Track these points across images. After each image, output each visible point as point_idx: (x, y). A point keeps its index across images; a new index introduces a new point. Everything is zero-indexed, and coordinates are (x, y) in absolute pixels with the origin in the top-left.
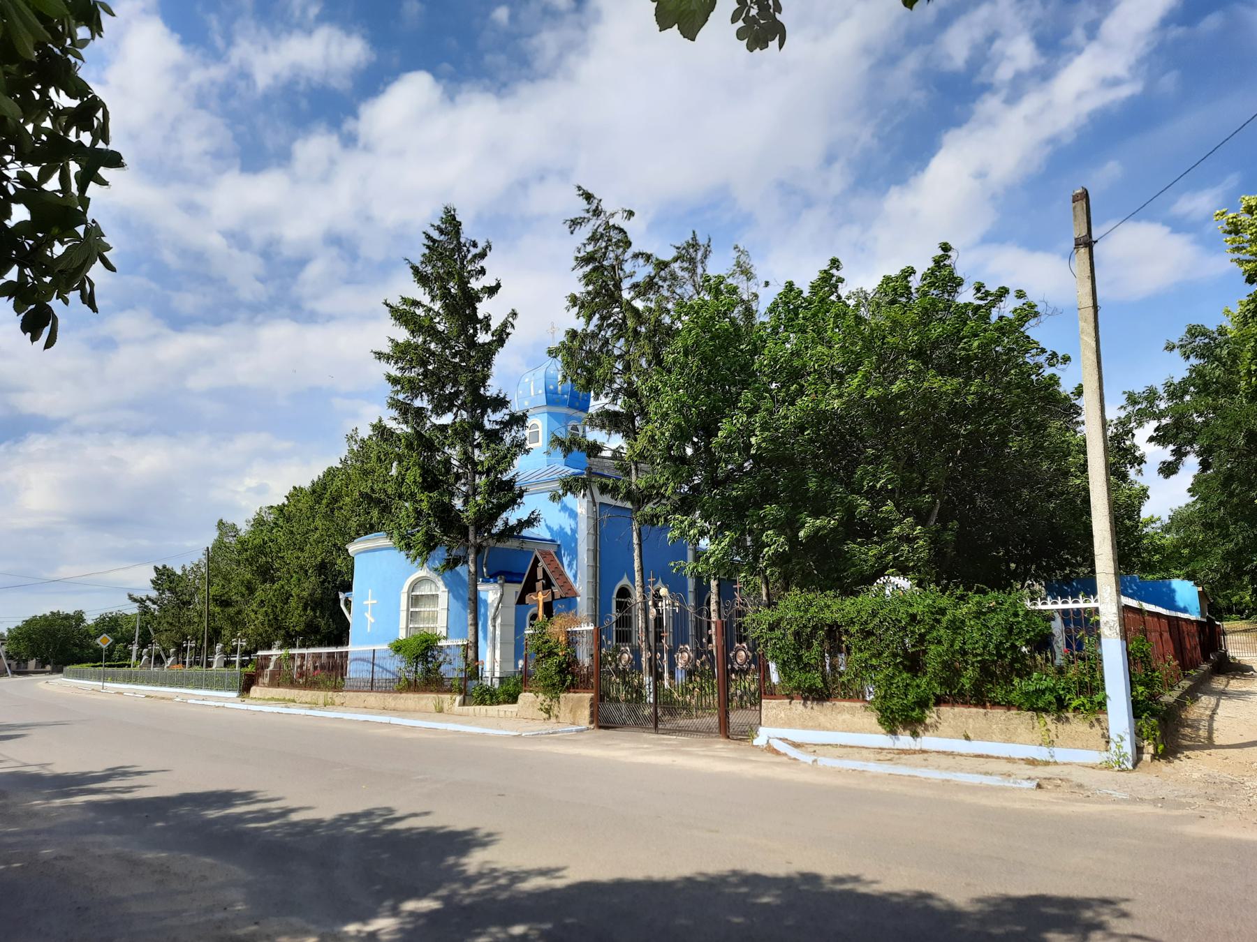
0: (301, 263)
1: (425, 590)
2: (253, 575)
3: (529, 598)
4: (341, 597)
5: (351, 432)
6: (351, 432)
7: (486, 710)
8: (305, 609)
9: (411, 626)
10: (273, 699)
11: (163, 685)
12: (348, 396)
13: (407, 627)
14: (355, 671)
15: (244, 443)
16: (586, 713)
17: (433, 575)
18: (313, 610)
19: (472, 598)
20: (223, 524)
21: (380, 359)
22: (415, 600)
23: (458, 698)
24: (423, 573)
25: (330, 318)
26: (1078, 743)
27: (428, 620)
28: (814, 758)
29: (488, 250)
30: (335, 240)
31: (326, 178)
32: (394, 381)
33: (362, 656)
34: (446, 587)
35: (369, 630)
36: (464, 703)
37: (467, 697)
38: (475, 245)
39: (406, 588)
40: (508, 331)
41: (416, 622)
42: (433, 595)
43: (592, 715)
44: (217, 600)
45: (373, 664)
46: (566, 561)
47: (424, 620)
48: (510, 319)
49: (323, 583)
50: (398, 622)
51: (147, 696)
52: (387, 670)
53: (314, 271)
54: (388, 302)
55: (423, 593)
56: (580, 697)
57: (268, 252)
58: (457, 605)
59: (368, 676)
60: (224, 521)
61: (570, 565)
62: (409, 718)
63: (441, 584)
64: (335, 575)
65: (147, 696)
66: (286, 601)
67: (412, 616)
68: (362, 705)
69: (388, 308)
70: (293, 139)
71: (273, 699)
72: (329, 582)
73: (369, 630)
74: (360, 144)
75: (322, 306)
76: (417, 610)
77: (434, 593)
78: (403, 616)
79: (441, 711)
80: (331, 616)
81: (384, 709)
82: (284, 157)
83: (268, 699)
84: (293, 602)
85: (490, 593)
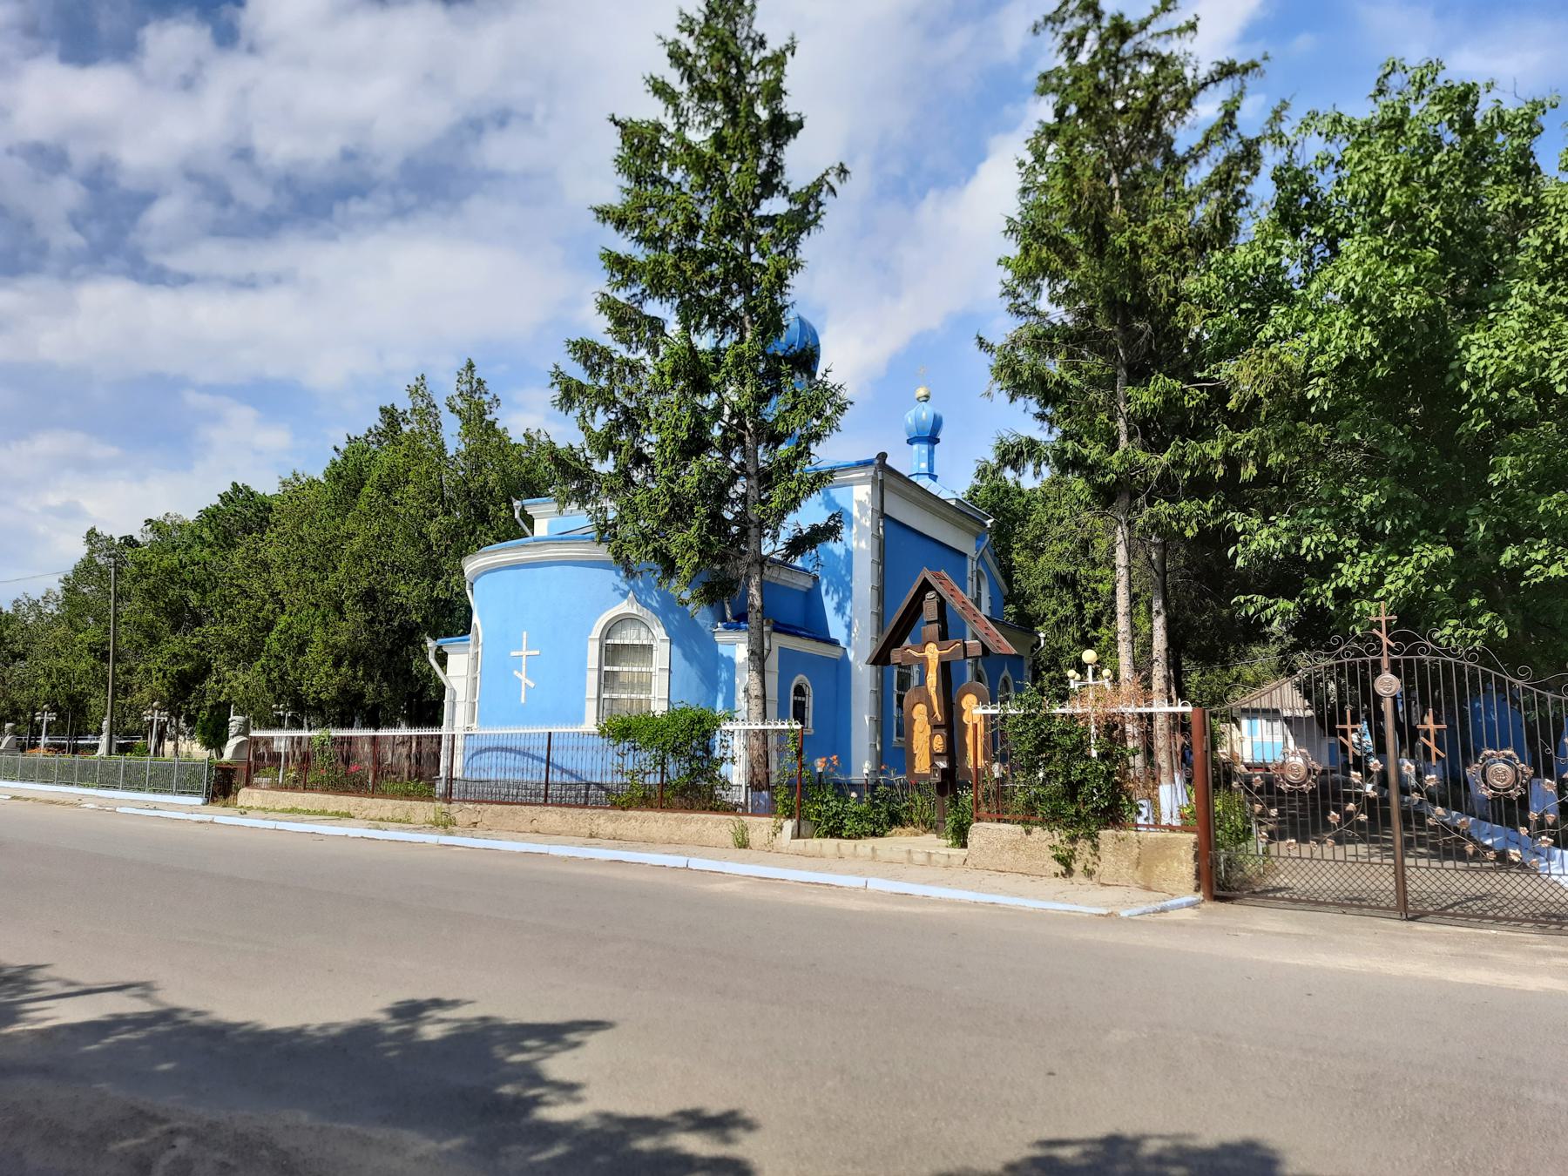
0: (146, 199)
1: (629, 637)
2: (157, 615)
3: (906, 651)
4: (429, 645)
5: (416, 383)
6: (416, 383)
7: (873, 849)
8: (337, 664)
9: (605, 696)
10: (293, 810)
11: (24, 779)
12: (210, 389)
13: (599, 697)
14: (456, 763)
15: (47, 444)
16: (1185, 867)
17: (645, 614)
18: (353, 665)
19: (758, 651)
20: (97, 535)
21: (604, 220)
22: (612, 653)
23: (789, 825)
24: (626, 607)
25: (186, 280)
26: (136, 786)
27: (631, 686)
28: (864, 880)
29: (788, 54)
30: (193, 174)
31: (189, 84)
32: (619, 265)
33: (504, 744)
34: (667, 635)
35: (523, 701)
36: (798, 835)
37: (803, 823)
38: (762, 43)
39: (596, 632)
40: (822, 197)
41: (612, 689)
42: (643, 646)
43: (1198, 875)
44: (96, 651)
45: (548, 764)
46: (829, 603)
47: (624, 686)
48: (832, 179)
49: (371, 621)
50: (582, 688)
51: (14, 798)
52: (567, 772)
53: (164, 213)
54: (617, 118)
55: (626, 642)
56: (1165, 840)
57: (99, 179)
58: (680, 663)
59: (536, 779)
60: (98, 531)
61: (840, 608)
62: (629, 850)
63: (660, 632)
64: (391, 612)
65: (14, 798)
66: (301, 650)
67: (607, 680)
68: (529, 828)
69: (618, 129)
70: (143, 23)
71: (293, 810)
72: (381, 623)
73: (523, 701)
74: (243, 44)
75: (176, 263)
76: (616, 669)
77: (645, 642)
78: (592, 679)
79: (743, 844)
80: (385, 676)
81: (591, 836)
82: (125, 49)
83: (315, 813)
84: (313, 654)
85: (737, 648)
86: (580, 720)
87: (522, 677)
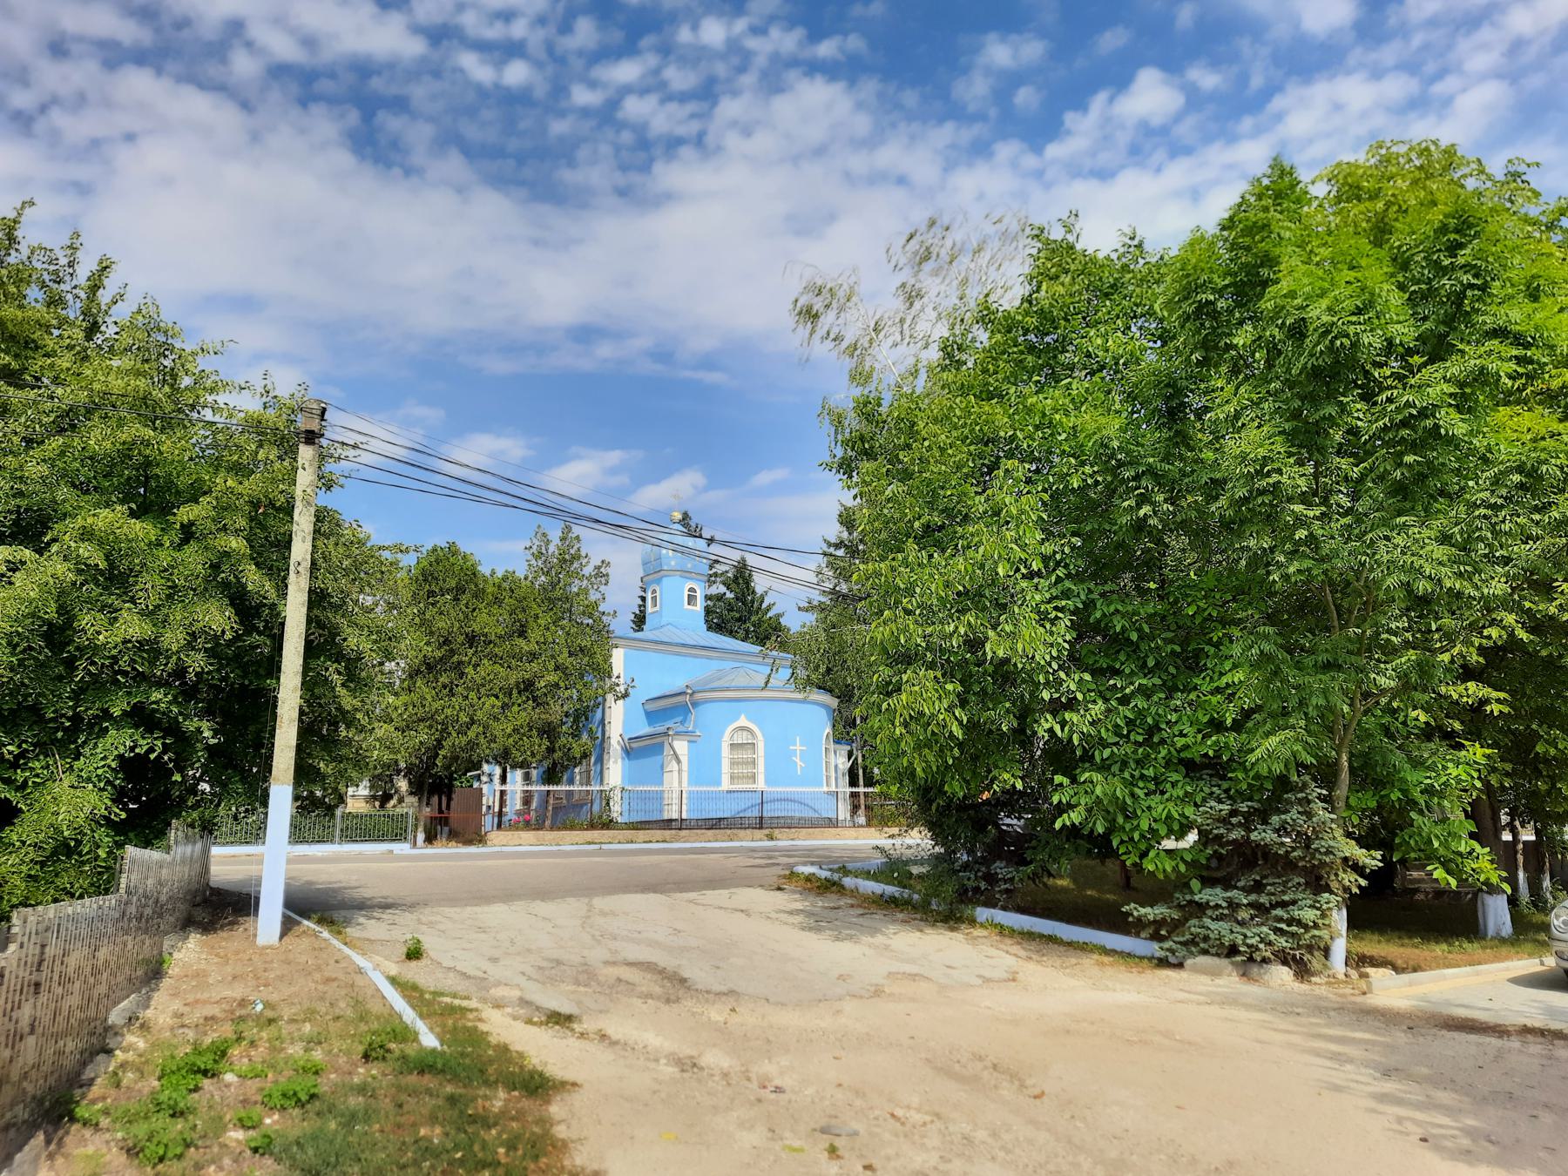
86: (719, 783)
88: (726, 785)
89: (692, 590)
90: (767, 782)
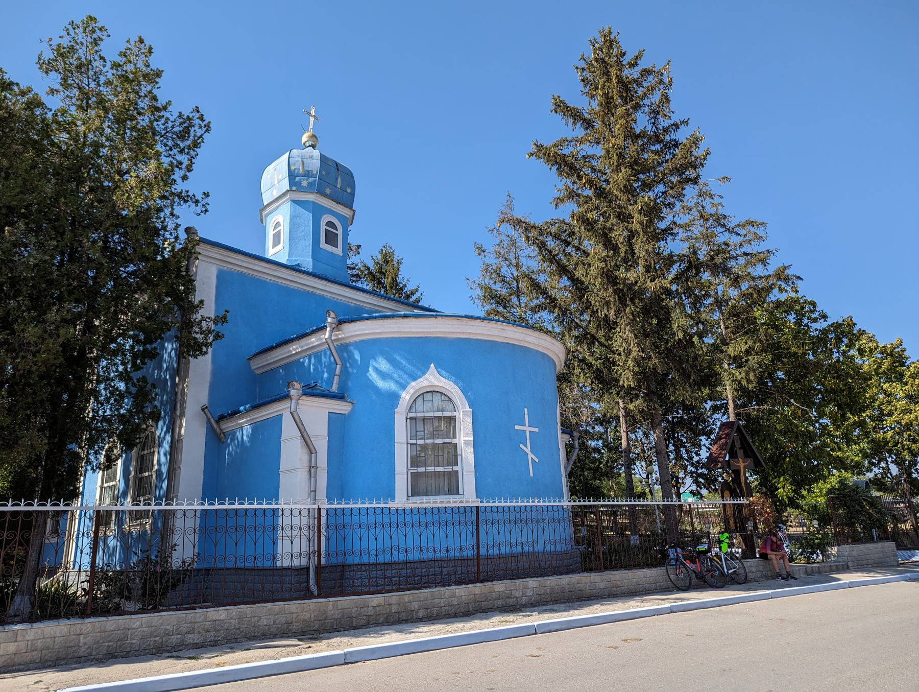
73: (532, 475)
86: (390, 494)
87: (528, 450)
88: (401, 500)
89: (330, 224)
90: (480, 492)
